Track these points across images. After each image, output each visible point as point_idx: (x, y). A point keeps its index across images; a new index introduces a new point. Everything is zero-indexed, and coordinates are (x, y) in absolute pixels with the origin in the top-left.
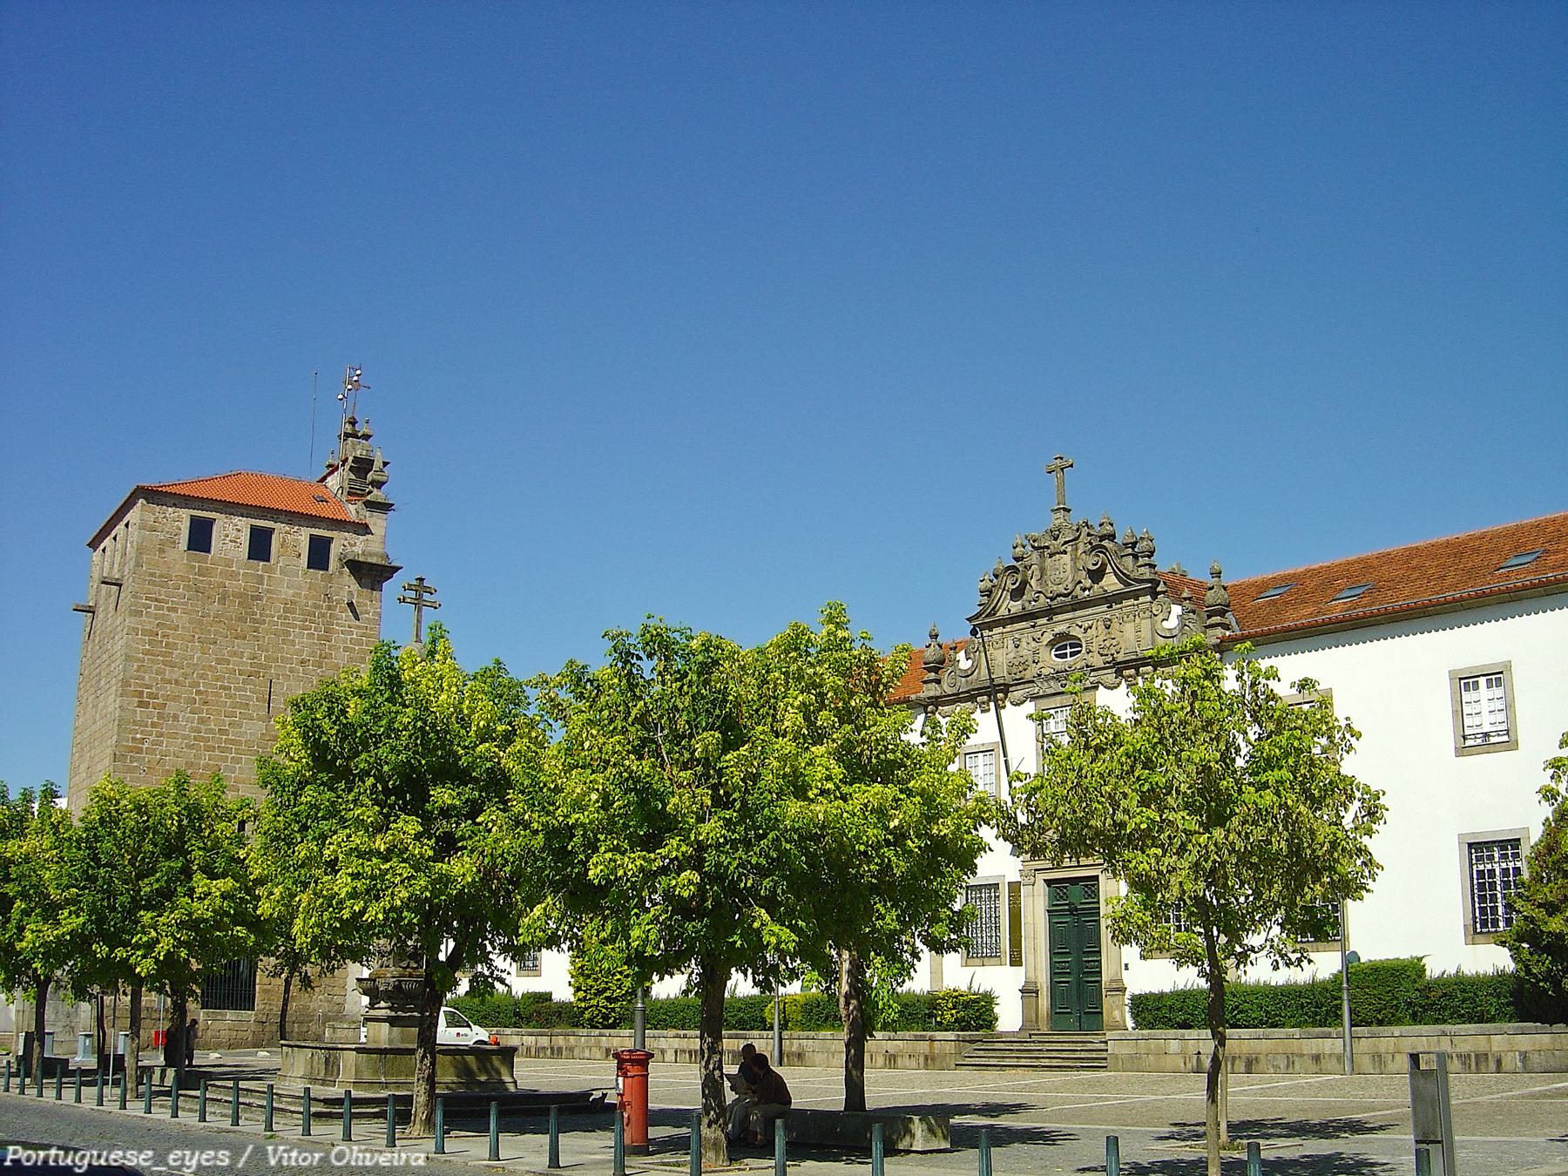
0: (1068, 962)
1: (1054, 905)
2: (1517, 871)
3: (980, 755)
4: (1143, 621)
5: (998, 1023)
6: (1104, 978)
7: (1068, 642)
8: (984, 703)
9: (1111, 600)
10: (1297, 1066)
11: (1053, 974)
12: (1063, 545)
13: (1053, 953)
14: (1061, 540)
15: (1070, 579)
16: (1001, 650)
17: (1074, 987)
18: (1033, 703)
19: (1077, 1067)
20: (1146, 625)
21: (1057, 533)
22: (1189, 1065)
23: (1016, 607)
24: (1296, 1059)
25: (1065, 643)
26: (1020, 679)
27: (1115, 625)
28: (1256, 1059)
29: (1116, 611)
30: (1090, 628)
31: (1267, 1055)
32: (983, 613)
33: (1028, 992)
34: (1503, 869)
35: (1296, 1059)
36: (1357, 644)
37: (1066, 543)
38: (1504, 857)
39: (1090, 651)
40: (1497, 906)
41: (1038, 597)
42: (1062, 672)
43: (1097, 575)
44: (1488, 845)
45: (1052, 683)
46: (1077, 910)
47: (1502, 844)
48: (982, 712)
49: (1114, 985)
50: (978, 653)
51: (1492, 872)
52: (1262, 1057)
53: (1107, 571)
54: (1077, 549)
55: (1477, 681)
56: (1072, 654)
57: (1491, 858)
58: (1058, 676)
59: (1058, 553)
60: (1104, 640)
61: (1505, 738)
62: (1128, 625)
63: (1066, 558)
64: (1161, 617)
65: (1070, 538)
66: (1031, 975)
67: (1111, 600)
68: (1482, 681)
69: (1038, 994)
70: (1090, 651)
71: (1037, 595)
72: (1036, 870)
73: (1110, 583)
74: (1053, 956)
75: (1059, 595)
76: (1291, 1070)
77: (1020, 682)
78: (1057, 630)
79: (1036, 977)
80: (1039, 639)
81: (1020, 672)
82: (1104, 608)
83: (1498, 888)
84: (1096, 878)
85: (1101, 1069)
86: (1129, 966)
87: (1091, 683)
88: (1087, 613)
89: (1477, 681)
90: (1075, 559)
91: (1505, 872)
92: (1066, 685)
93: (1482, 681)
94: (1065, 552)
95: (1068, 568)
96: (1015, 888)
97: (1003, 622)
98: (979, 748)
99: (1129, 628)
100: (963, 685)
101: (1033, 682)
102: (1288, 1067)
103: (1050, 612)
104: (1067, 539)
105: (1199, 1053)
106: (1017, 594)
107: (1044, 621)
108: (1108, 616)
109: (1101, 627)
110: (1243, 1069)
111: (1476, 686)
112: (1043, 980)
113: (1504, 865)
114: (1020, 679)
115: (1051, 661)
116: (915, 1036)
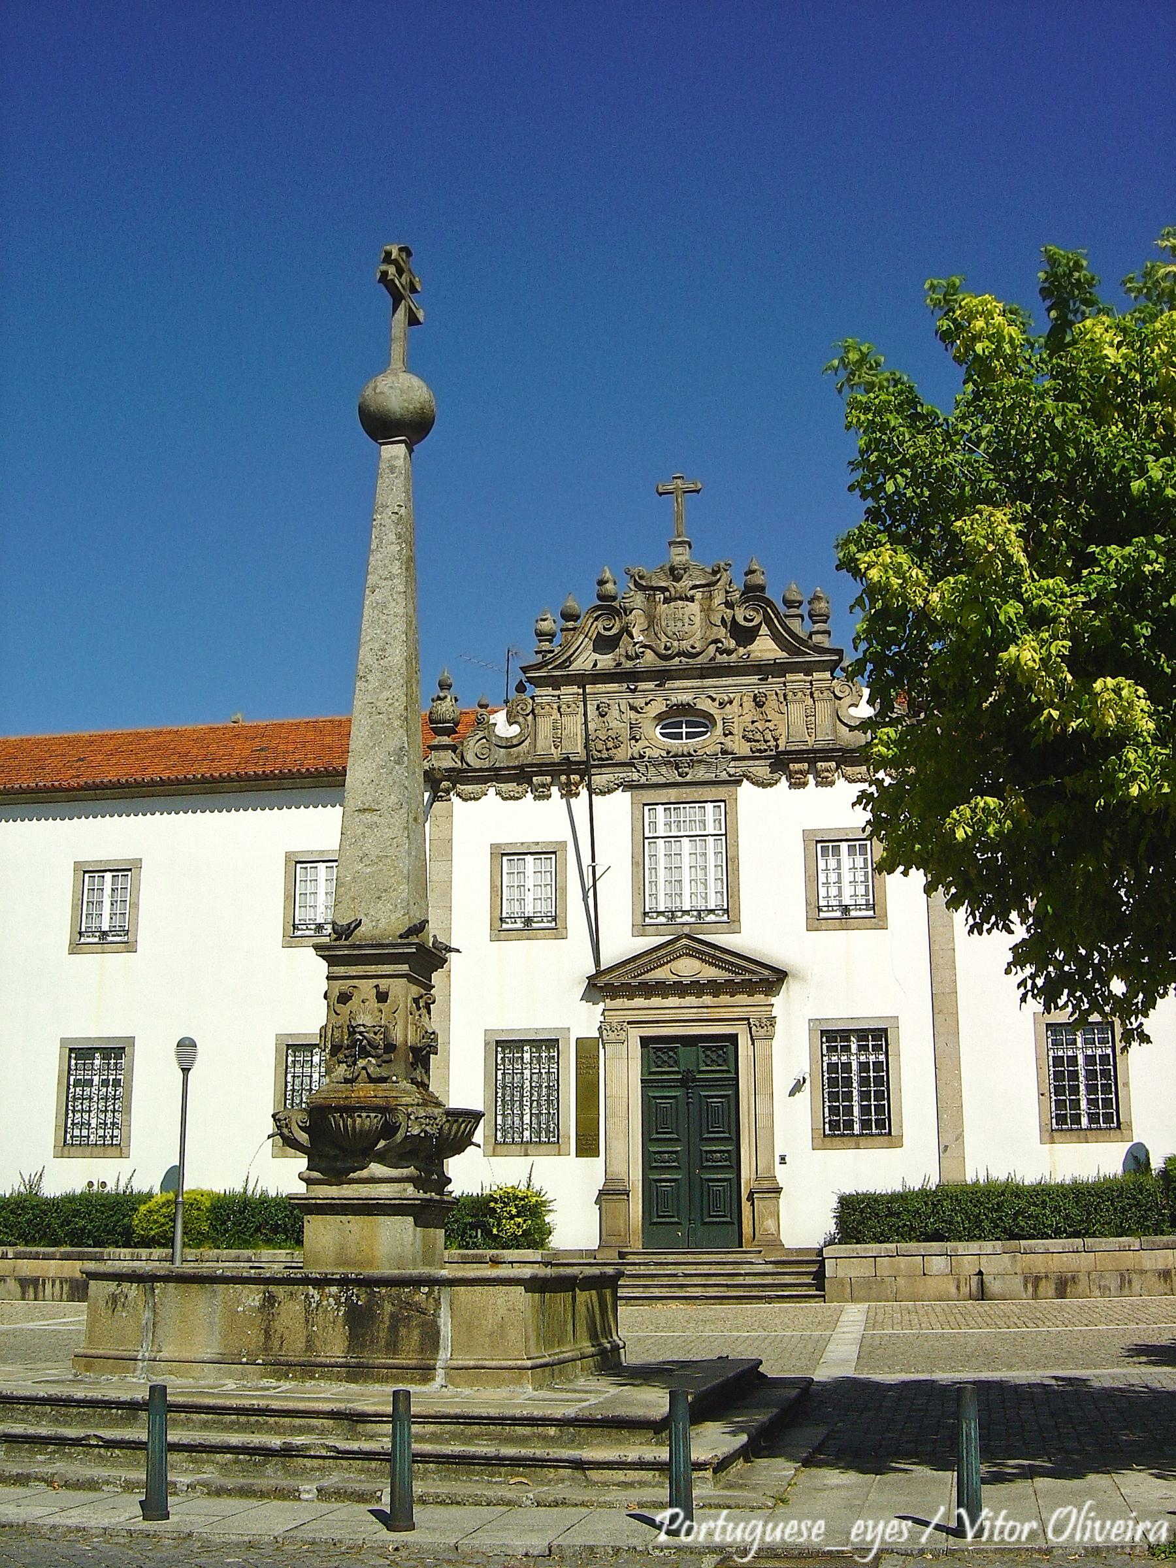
0: (676, 1152)
3: (529, 858)
5: (550, 1237)
8: (544, 786)
9: (765, 670)
10: (1136, 1286)
11: (647, 1167)
12: (691, 589)
13: (647, 1139)
14: (686, 583)
15: (699, 635)
17: (684, 1189)
18: (629, 794)
19: (769, 1297)
20: (824, 710)
21: (682, 572)
22: (965, 1290)
23: (606, 661)
24: (1134, 1277)
25: (679, 719)
26: (607, 759)
27: (772, 704)
28: (1073, 1278)
30: (731, 702)
31: (1089, 1273)
32: (551, 663)
34: (1087, 1056)
35: (1134, 1277)
36: (254, 810)
37: (694, 587)
38: (862, 1048)
39: (731, 733)
40: (1079, 1100)
41: (643, 653)
42: (683, 755)
43: (745, 635)
44: (845, 1034)
45: (663, 770)
46: (695, 1080)
47: (862, 1034)
48: (536, 798)
49: (766, 1185)
51: (847, 1067)
52: (1082, 1277)
53: (760, 633)
54: (711, 598)
55: (125, 870)
56: (690, 736)
57: (847, 1049)
58: (674, 761)
59: (681, 599)
60: (753, 722)
61: (871, 913)
63: (694, 608)
64: (847, 701)
65: (703, 582)
66: (619, 1169)
67: (765, 670)
68: (844, 846)
69: (628, 1196)
70: (731, 733)
71: (641, 650)
72: (629, 1023)
73: (765, 648)
74: (648, 1144)
75: (679, 654)
76: (1126, 1291)
77: (607, 763)
78: (674, 700)
80: (641, 708)
82: (754, 679)
83: (855, 1085)
84: (733, 1039)
85: (811, 1300)
86: (787, 1159)
87: (730, 776)
88: (728, 683)
90: (707, 610)
91: (864, 1067)
92: (687, 774)
93: (844, 846)
94: (692, 599)
95: (697, 620)
96: (587, 1051)
97: (581, 680)
98: (529, 847)
99: (796, 712)
100: (500, 758)
101: (633, 765)
102: (1121, 1287)
103: (662, 676)
104: (698, 583)
105: (980, 1273)
106: (604, 644)
107: (651, 685)
108: (764, 690)
109: (749, 704)
110: (1051, 1291)
111: (836, 851)
113: (863, 1059)
114: (607, 759)
115: (655, 740)
116: (463, 1256)
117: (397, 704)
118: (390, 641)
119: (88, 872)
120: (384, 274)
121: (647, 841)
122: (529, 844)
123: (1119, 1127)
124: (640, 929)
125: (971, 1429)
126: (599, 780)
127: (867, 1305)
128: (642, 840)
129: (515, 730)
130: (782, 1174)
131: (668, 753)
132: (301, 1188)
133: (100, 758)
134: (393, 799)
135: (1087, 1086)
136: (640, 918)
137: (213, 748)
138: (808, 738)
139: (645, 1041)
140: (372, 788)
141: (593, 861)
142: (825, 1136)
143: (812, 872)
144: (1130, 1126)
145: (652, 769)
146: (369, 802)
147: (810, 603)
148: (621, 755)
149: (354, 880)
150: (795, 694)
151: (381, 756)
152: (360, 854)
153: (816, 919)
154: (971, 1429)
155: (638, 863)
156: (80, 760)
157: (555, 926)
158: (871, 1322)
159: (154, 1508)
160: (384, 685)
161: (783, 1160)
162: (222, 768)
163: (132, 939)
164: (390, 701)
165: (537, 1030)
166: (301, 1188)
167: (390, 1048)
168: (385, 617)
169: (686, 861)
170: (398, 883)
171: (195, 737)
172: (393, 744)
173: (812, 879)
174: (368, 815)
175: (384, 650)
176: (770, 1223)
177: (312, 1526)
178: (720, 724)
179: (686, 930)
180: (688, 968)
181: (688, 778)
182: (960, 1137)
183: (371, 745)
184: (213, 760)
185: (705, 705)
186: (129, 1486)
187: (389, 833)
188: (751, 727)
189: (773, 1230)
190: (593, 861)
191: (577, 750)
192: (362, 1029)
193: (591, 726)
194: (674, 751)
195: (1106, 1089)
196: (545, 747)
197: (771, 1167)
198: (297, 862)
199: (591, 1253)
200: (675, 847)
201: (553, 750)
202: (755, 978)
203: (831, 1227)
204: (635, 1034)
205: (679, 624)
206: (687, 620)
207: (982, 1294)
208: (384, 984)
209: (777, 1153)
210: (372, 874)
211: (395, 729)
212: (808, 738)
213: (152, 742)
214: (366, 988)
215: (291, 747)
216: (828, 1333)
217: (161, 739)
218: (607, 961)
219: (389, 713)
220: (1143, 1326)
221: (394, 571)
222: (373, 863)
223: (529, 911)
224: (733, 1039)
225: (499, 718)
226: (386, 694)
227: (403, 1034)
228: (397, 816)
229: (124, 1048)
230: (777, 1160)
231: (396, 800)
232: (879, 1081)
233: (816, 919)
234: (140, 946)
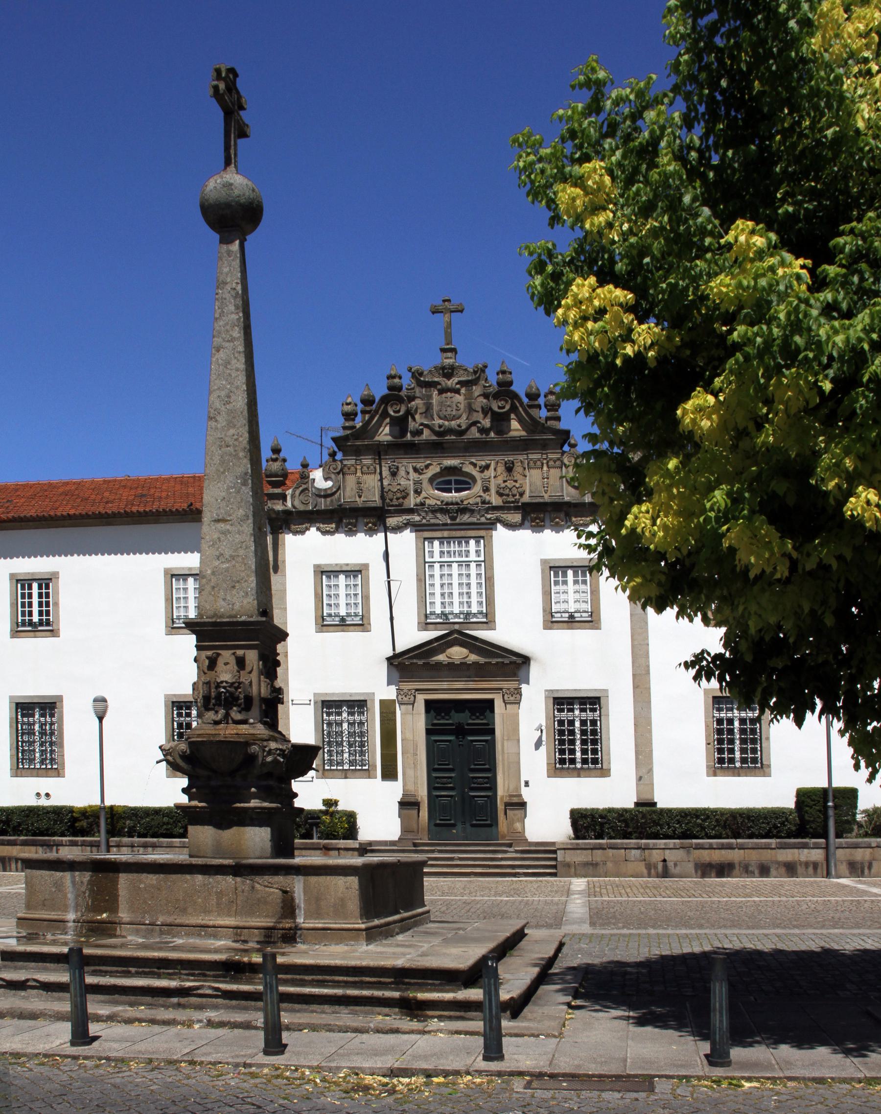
1: (433, 725)
2: (42, 715)
4: (552, 471)
6: (500, 792)
7: (453, 478)
13: (430, 769)
16: (373, 476)
27: (518, 468)
29: (519, 458)
33: (407, 804)
45: (439, 515)
49: (515, 800)
50: (341, 475)
55: (46, 582)
58: (442, 509)
62: (533, 472)
63: (459, 398)
66: (411, 787)
72: (417, 690)
79: (417, 791)
81: (398, 499)
86: (530, 784)
89: (46, 582)
96: (387, 708)
105: (664, 861)
109: (501, 469)
111: (565, 575)
112: (423, 793)
117: (241, 439)
118: (234, 390)
119: (23, 583)
120: (216, 88)
121: (427, 565)
122: (341, 565)
123: (762, 767)
124: (425, 625)
125: (719, 993)
126: (392, 521)
127: (586, 880)
128: (423, 565)
129: (329, 484)
130: (526, 794)
131: (442, 502)
132: (184, 799)
133: (24, 500)
134: (241, 512)
135: (741, 739)
136: (423, 618)
137: (107, 494)
138: (544, 494)
139: (429, 704)
140: (224, 504)
141: (388, 576)
142: (556, 768)
143: (548, 588)
144: (769, 766)
145: (431, 515)
146: (222, 514)
147: (545, 396)
148: (412, 501)
149: (213, 573)
150: (535, 463)
151: (230, 479)
152: (217, 553)
153: (551, 622)
154: (719, 993)
155: (421, 580)
156: (8, 501)
157: (363, 625)
158: (590, 892)
159: (82, 1036)
160: (230, 424)
161: (527, 784)
162: (111, 508)
163: (55, 627)
164: (236, 437)
165: (351, 695)
166: (184, 799)
167: (249, 700)
168: (228, 371)
169: (455, 581)
170: (248, 576)
171: (93, 487)
172: (240, 470)
173: (547, 594)
174: (221, 525)
175: (229, 397)
176: (518, 825)
177: (203, 1050)
178: (479, 482)
179: (457, 627)
180: (457, 653)
181: (458, 521)
182: (650, 771)
183: (222, 470)
184: (107, 503)
185: (468, 469)
186: (59, 1017)
187: (238, 538)
188: (503, 485)
189: (520, 830)
190: (388, 576)
191: (375, 499)
192: (224, 684)
193: (385, 483)
194: (446, 500)
195: (595, 742)
196: (349, 495)
197: (518, 788)
198: (174, 576)
199: (393, 843)
200: (446, 571)
201: (358, 499)
202: (507, 661)
203: (570, 831)
204: (421, 698)
205: (449, 409)
206: (455, 407)
207: (666, 874)
208: (240, 652)
209: (523, 779)
210: (227, 570)
211: (240, 458)
212: (544, 494)
213: (61, 490)
214: (226, 655)
215: (164, 494)
216: (564, 898)
217: (67, 488)
218: (400, 648)
219: (235, 446)
220: (784, 899)
221: (234, 335)
222: (228, 561)
223: (343, 612)
224: (491, 702)
225: (317, 475)
226: (232, 431)
227: (259, 688)
228: (245, 526)
229: (55, 703)
230: (523, 784)
231: (244, 513)
232: (594, 732)
233: (551, 622)
234: (62, 633)
